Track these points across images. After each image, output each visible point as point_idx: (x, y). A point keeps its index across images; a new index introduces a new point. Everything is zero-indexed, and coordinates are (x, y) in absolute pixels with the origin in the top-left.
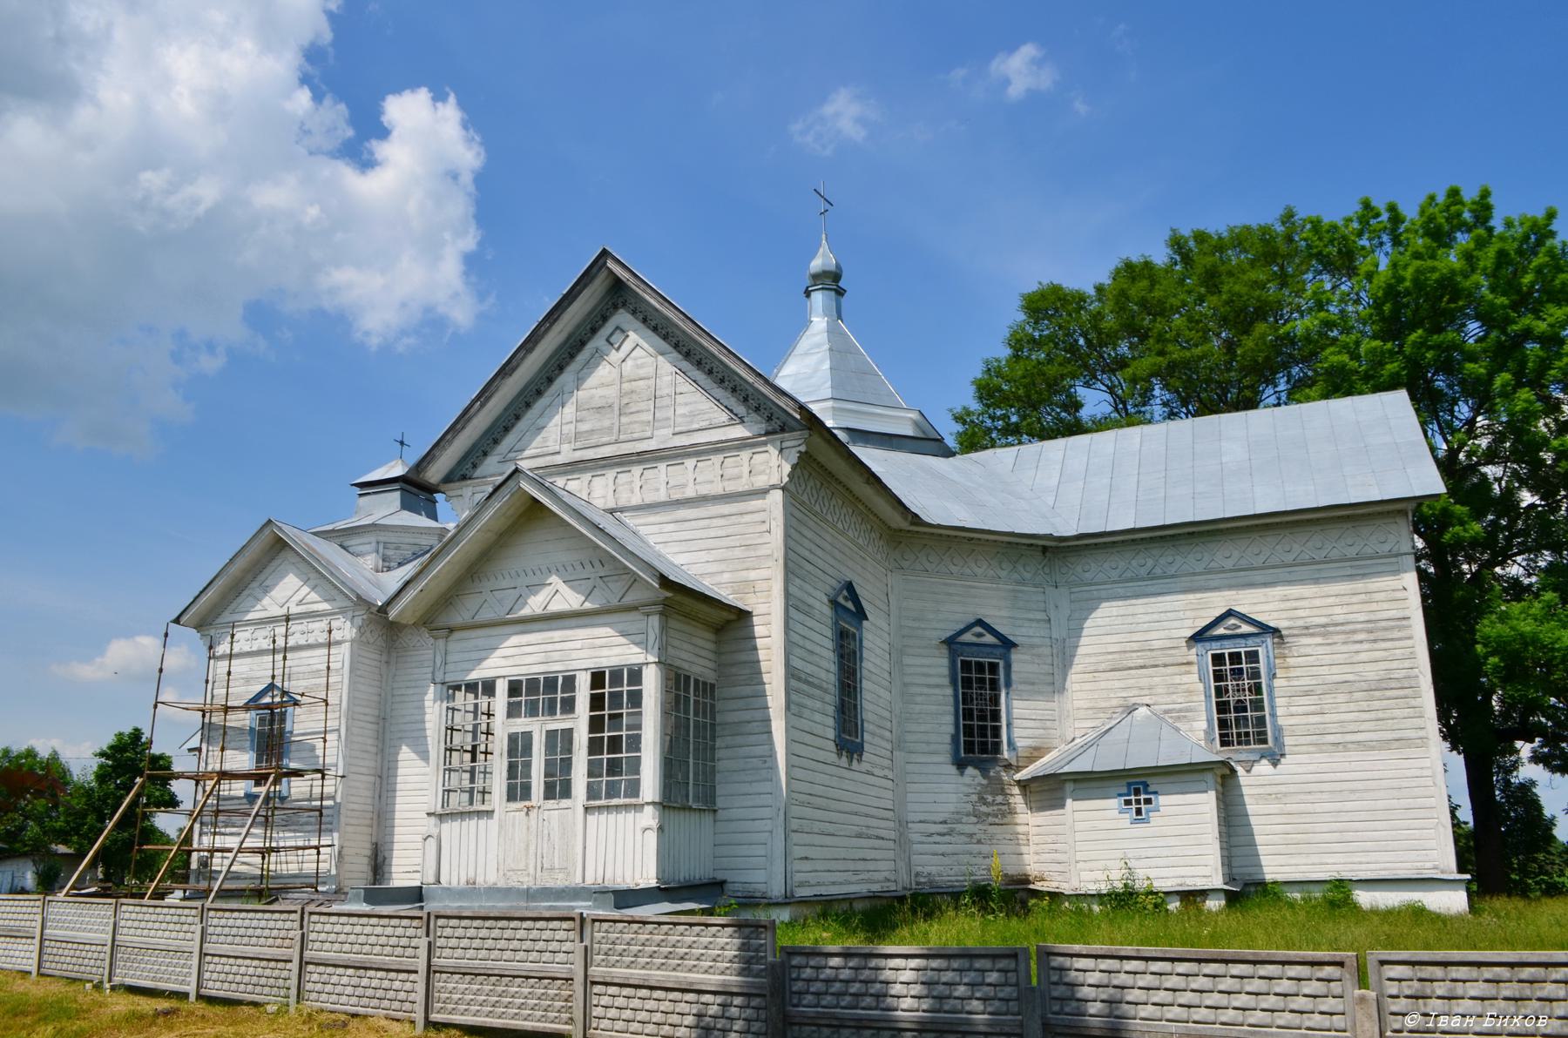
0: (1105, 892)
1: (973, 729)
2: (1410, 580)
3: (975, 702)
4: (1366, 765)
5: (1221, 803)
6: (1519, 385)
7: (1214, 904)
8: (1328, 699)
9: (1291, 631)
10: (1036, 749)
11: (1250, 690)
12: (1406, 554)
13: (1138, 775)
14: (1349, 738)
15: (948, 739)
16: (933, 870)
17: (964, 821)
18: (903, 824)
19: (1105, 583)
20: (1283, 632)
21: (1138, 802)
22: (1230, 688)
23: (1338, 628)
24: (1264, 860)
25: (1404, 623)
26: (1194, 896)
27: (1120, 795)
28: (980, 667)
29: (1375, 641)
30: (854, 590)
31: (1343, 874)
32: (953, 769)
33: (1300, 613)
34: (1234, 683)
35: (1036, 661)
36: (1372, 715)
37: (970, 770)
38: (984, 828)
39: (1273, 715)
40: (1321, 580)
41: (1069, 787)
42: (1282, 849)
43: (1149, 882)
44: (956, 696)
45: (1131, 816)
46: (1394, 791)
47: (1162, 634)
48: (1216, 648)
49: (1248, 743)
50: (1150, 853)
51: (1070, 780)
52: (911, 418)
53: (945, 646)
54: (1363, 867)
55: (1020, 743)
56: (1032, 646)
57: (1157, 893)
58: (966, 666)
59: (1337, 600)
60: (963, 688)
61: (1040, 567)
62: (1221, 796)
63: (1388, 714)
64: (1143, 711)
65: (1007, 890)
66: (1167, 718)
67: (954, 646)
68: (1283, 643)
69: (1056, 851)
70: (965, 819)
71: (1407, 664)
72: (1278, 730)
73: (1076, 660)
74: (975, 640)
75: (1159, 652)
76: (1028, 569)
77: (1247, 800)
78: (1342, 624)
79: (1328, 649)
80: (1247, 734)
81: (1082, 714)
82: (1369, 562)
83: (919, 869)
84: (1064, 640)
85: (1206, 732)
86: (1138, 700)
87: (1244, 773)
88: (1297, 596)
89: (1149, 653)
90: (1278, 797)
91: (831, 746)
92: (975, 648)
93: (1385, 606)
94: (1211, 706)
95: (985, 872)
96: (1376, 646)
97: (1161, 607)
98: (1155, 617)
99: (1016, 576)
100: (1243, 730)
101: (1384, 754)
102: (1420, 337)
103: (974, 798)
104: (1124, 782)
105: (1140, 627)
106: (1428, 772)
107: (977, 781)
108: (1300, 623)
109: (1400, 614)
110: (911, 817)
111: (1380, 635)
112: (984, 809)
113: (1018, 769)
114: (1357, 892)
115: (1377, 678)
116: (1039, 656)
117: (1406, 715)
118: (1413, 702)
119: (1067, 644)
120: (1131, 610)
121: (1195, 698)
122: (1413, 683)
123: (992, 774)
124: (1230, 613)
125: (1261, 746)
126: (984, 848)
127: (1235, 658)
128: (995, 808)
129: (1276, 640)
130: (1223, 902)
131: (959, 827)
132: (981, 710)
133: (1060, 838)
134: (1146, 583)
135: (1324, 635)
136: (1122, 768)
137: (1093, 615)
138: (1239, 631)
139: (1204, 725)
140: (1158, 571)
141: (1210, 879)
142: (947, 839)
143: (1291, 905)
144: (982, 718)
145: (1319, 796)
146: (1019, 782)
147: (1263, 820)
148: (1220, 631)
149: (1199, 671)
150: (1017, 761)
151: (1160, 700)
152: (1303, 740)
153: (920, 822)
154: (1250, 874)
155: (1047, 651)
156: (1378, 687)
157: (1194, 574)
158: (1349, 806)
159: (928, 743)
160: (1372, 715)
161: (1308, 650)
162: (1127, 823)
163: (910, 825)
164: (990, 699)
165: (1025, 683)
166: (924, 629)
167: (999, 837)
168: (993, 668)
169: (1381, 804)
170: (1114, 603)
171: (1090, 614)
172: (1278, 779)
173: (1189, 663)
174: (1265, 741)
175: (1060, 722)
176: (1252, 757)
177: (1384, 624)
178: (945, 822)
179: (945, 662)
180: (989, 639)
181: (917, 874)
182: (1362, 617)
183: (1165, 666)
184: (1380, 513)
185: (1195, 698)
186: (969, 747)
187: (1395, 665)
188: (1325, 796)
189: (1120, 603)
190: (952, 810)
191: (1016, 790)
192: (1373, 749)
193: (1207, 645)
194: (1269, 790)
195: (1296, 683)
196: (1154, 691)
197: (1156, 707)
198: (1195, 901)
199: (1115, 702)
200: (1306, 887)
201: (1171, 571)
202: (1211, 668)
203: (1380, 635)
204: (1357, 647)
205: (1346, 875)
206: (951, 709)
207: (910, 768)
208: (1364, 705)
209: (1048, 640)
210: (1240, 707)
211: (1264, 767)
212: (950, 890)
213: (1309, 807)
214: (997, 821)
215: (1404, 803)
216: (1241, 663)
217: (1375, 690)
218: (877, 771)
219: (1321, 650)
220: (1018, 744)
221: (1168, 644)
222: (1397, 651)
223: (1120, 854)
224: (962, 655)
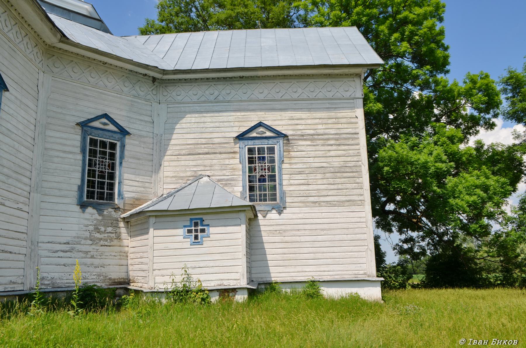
0: (170, 290)
1: (95, 183)
2: (360, 113)
3: (97, 166)
4: (331, 215)
5: (248, 234)
6: (402, 40)
7: (241, 297)
8: (312, 176)
9: (294, 137)
10: (137, 199)
11: (269, 169)
12: (358, 98)
13: (198, 214)
14: (322, 199)
15: (76, 188)
16: (56, 275)
17: (82, 243)
18: (34, 244)
19: (189, 103)
20: (289, 137)
21: (196, 231)
22: (257, 168)
23: (320, 137)
24: (272, 269)
25: (355, 136)
26: (228, 292)
27: (185, 226)
28: (103, 144)
29: (339, 145)
31: (315, 277)
32: (78, 208)
33: (299, 127)
34: (260, 165)
35: (142, 146)
36: (335, 187)
37: (90, 210)
38: (97, 248)
39: (281, 184)
40: (312, 110)
41: (152, 220)
42: (281, 263)
43: (200, 283)
44: (84, 161)
45: (191, 240)
46: (345, 230)
47: (220, 135)
48: (251, 144)
49: (265, 200)
50: (202, 264)
51: (153, 216)
52: (87, 9)
53: (79, 127)
54: (326, 273)
55: (127, 195)
56: (141, 136)
57: (204, 291)
58: (93, 142)
59: (320, 121)
60: (89, 156)
61: (150, 90)
62: (248, 230)
63: (344, 186)
64: (206, 179)
65: (109, 288)
66: (219, 184)
67: (85, 128)
68: (289, 144)
69: (142, 263)
70: (83, 242)
71: (355, 159)
72: (283, 193)
73: (170, 147)
74: (102, 126)
75: (218, 145)
76: (142, 89)
77: (263, 234)
78: (322, 135)
79: (313, 148)
80: (265, 195)
81: (169, 180)
82: (338, 101)
83: (45, 275)
84: (161, 135)
85: (242, 193)
86: (203, 173)
87: (262, 218)
88: (299, 117)
89: (212, 146)
90: (281, 232)
92: (101, 132)
93: (346, 126)
94: (245, 178)
95: (95, 277)
96: (340, 148)
97: (221, 119)
98: (217, 124)
99: (134, 92)
100: (263, 193)
101: (340, 209)
102: (361, 10)
103: (91, 228)
104: (188, 218)
105: (207, 130)
106: (364, 220)
107: (94, 217)
108: (299, 133)
109: (353, 131)
110: (42, 239)
111: (342, 142)
112: (98, 235)
113: (125, 211)
114: (322, 288)
115: (339, 166)
116: (145, 143)
117: (353, 187)
118: (358, 180)
119: (163, 138)
120: (203, 120)
121: (237, 173)
122: (358, 169)
123: (105, 213)
124: (260, 124)
125: (273, 202)
126: (96, 262)
128: (106, 235)
129: (285, 142)
130: (246, 296)
131: (78, 247)
132: (102, 172)
133: (145, 255)
134: (213, 104)
135: (311, 140)
137: (181, 122)
138: (264, 135)
139: (240, 189)
140: (221, 98)
141: (239, 281)
142: (68, 254)
143: (287, 298)
144: (102, 176)
145: (303, 232)
146: (124, 218)
147: (271, 246)
148: (254, 134)
149: (240, 157)
150: (124, 206)
151: (216, 173)
152: (296, 199)
153: (49, 242)
154: (262, 278)
155: (150, 140)
156: (340, 171)
157: (241, 101)
158: (320, 238)
159: (60, 190)
160: (335, 187)
161: (303, 148)
162: (188, 245)
163: (40, 244)
165: (134, 158)
166: (65, 114)
167: (107, 254)
168: (113, 146)
169: (337, 237)
170: (193, 115)
171: (179, 121)
173: (234, 153)
174: (275, 200)
175: (155, 184)
176: (267, 208)
177: (344, 136)
178: (68, 243)
179: (79, 138)
180: (111, 127)
181: (43, 279)
182: (333, 131)
183: (220, 153)
184: (347, 75)
185: (237, 173)
186: (91, 195)
187: (349, 159)
188: (307, 232)
189: (197, 115)
190: (75, 235)
191: (122, 224)
192: (335, 206)
193: (246, 142)
194: (276, 228)
195: (295, 167)
196: (212, 168)
197: (213, 177)
198: (229, 295)
199: (189, 174)
200: (293, 285)
201: (229, 98)
202: (247, 156)
203: (342, 142)
204: (329, 148)
205: (317, 278)
206: (80, 169)
207: (43, 205)
208: (331, 181)
209: (151, 134)
210: (262, 179)
211: (273, 215)
212: (66, 289)
213: (298, 239)
214: (106, 243)
215: (350, 237)
216: (264, 154)
217: (338, 172)
218: (7, 203)
219: (309, 148)
220: (126, 196)
221: (223, 140)
222: (351, 151)
223: (182, 265)
224: (91, 134)
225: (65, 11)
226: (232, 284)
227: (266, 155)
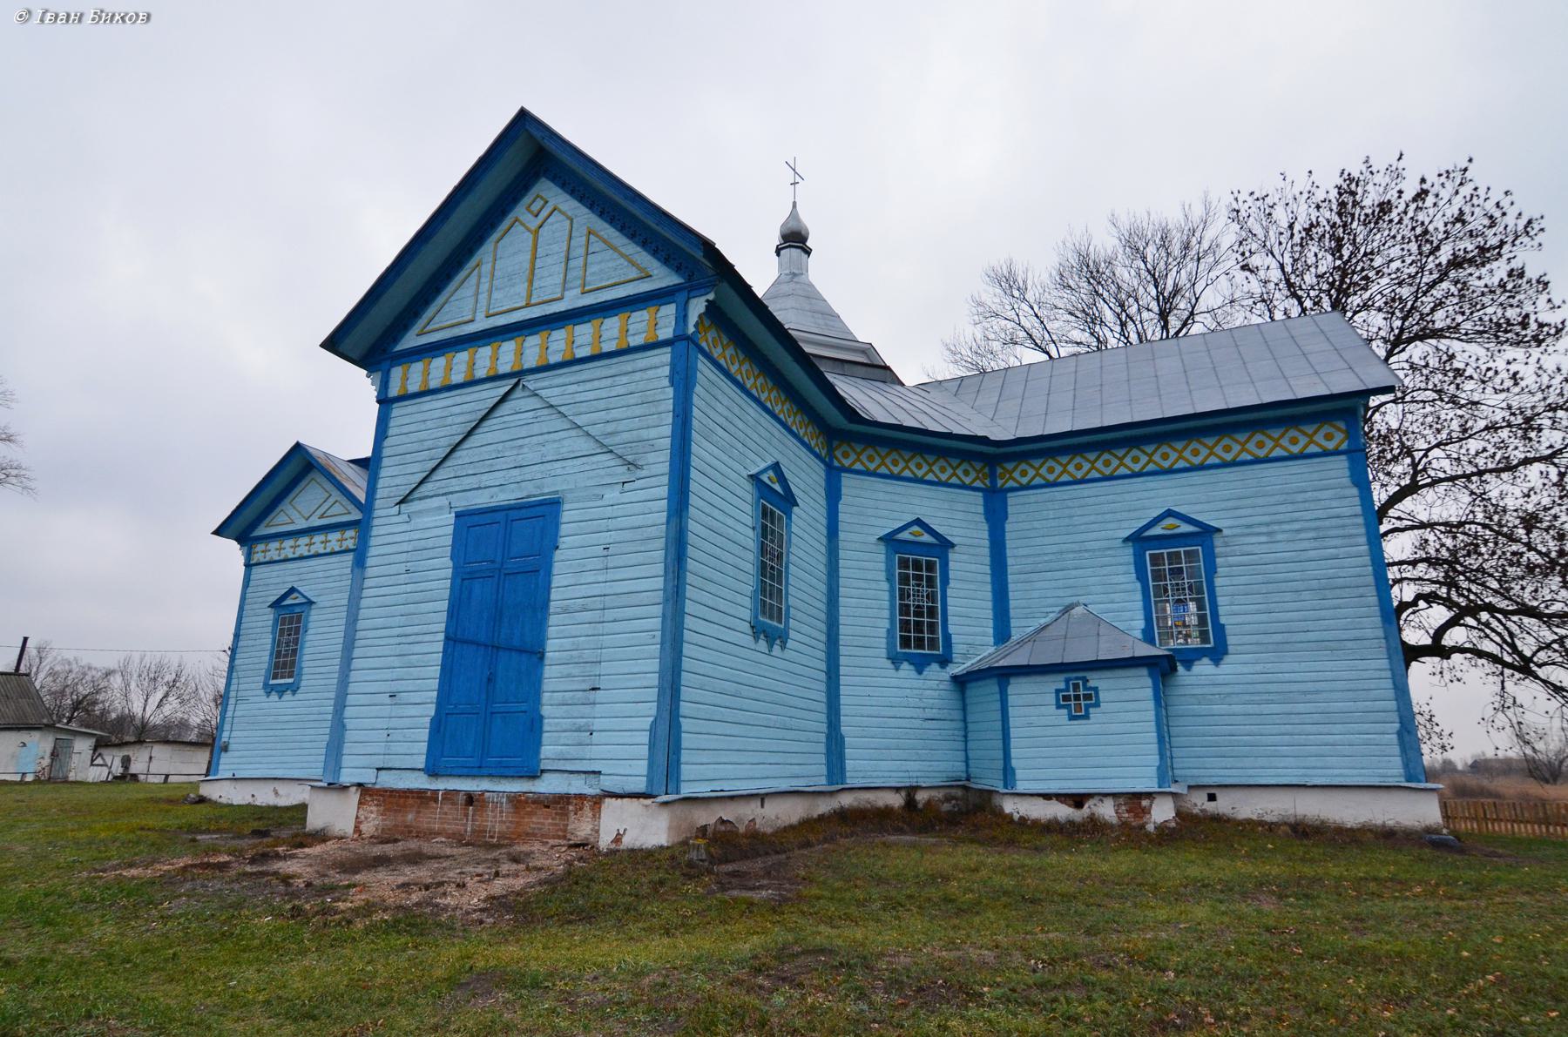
32: (888, 664)
53: (882, 543)
64: (1079, 610)
74: (911, 538)
91: (746, 627)
104: (1062, 677)
132: (918, 606)
135: (1269, 534)
136: (1060, 661)
164: (928, 595)
168: (930, 567)
172: (1220, 679)
180: (927, 538)
186: (905, 642)
219: (1265, 548)
225: (837, 363)
226: (1140, 787)
227: (1184, 565)
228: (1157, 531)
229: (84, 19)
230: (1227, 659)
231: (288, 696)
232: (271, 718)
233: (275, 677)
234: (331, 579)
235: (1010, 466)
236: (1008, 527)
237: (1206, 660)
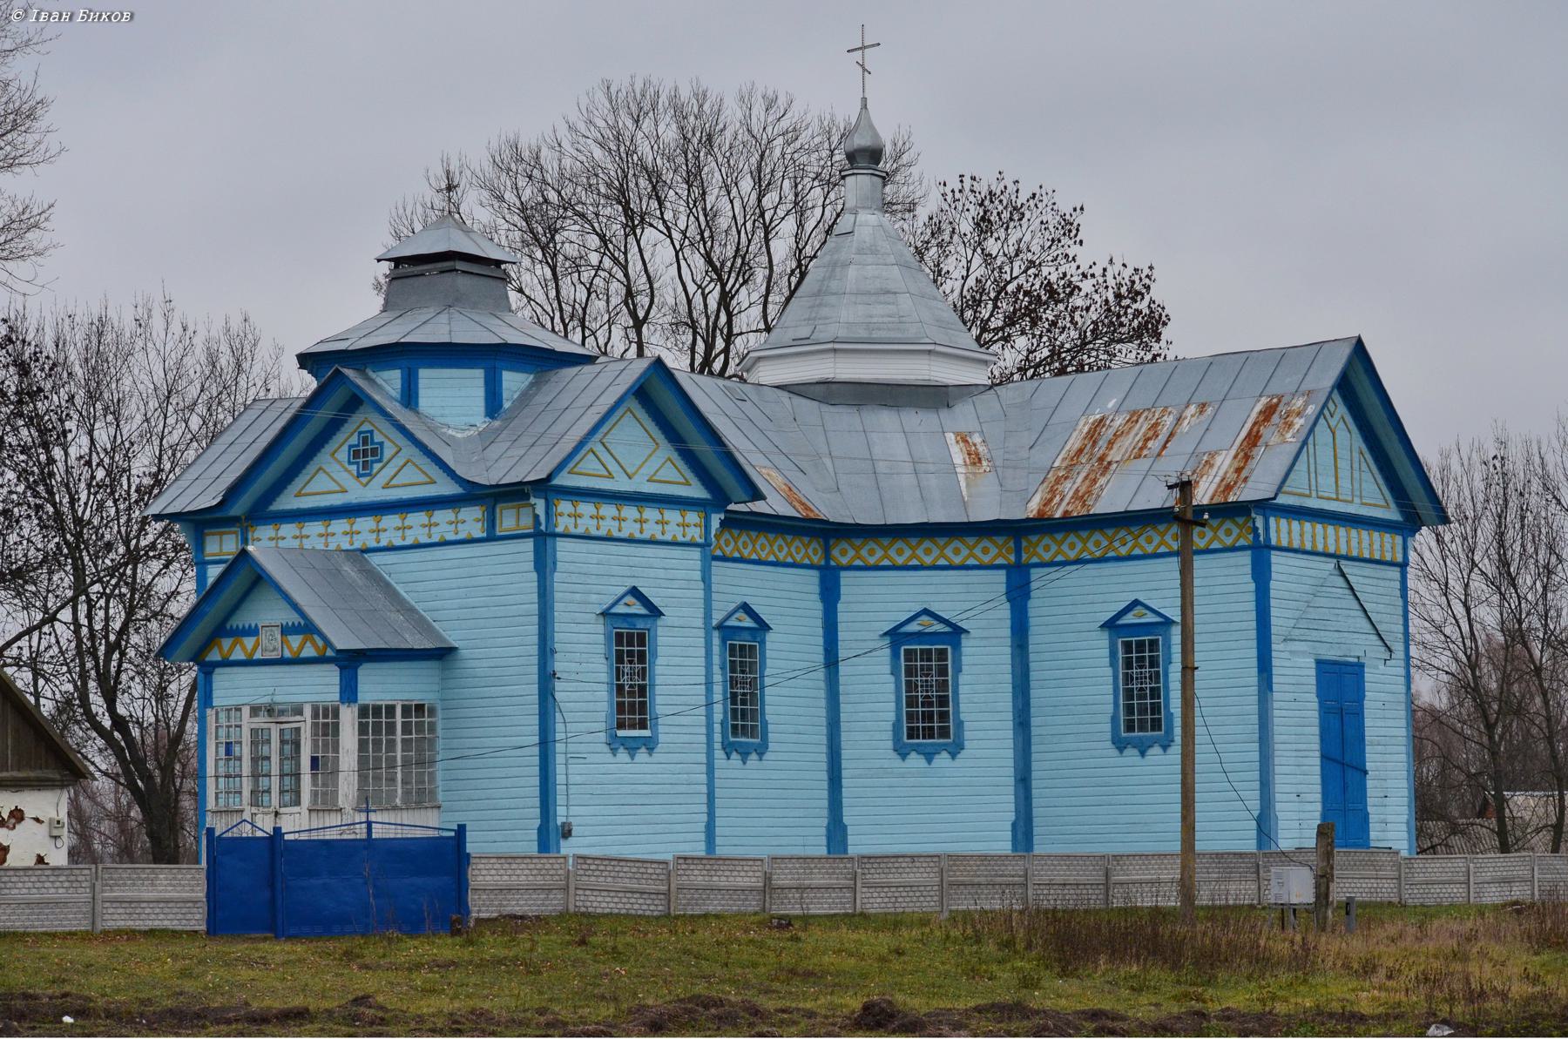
15: (889, 726)
30: (652, 603)
44: (1115, 678)
124: (1136, 603)
127: (1140, 645)
164: (1132, 680)
174: (910, 736)
186: (912, 733)
228: (913, 627)
229: (74, 17)
230: (963, 754)
231: (642, 756)
232: (627, 789)
233: (621, 726)
234: (676, 584)
235: (1034, 538)
236: (840, 606)
237: (945, 755)
